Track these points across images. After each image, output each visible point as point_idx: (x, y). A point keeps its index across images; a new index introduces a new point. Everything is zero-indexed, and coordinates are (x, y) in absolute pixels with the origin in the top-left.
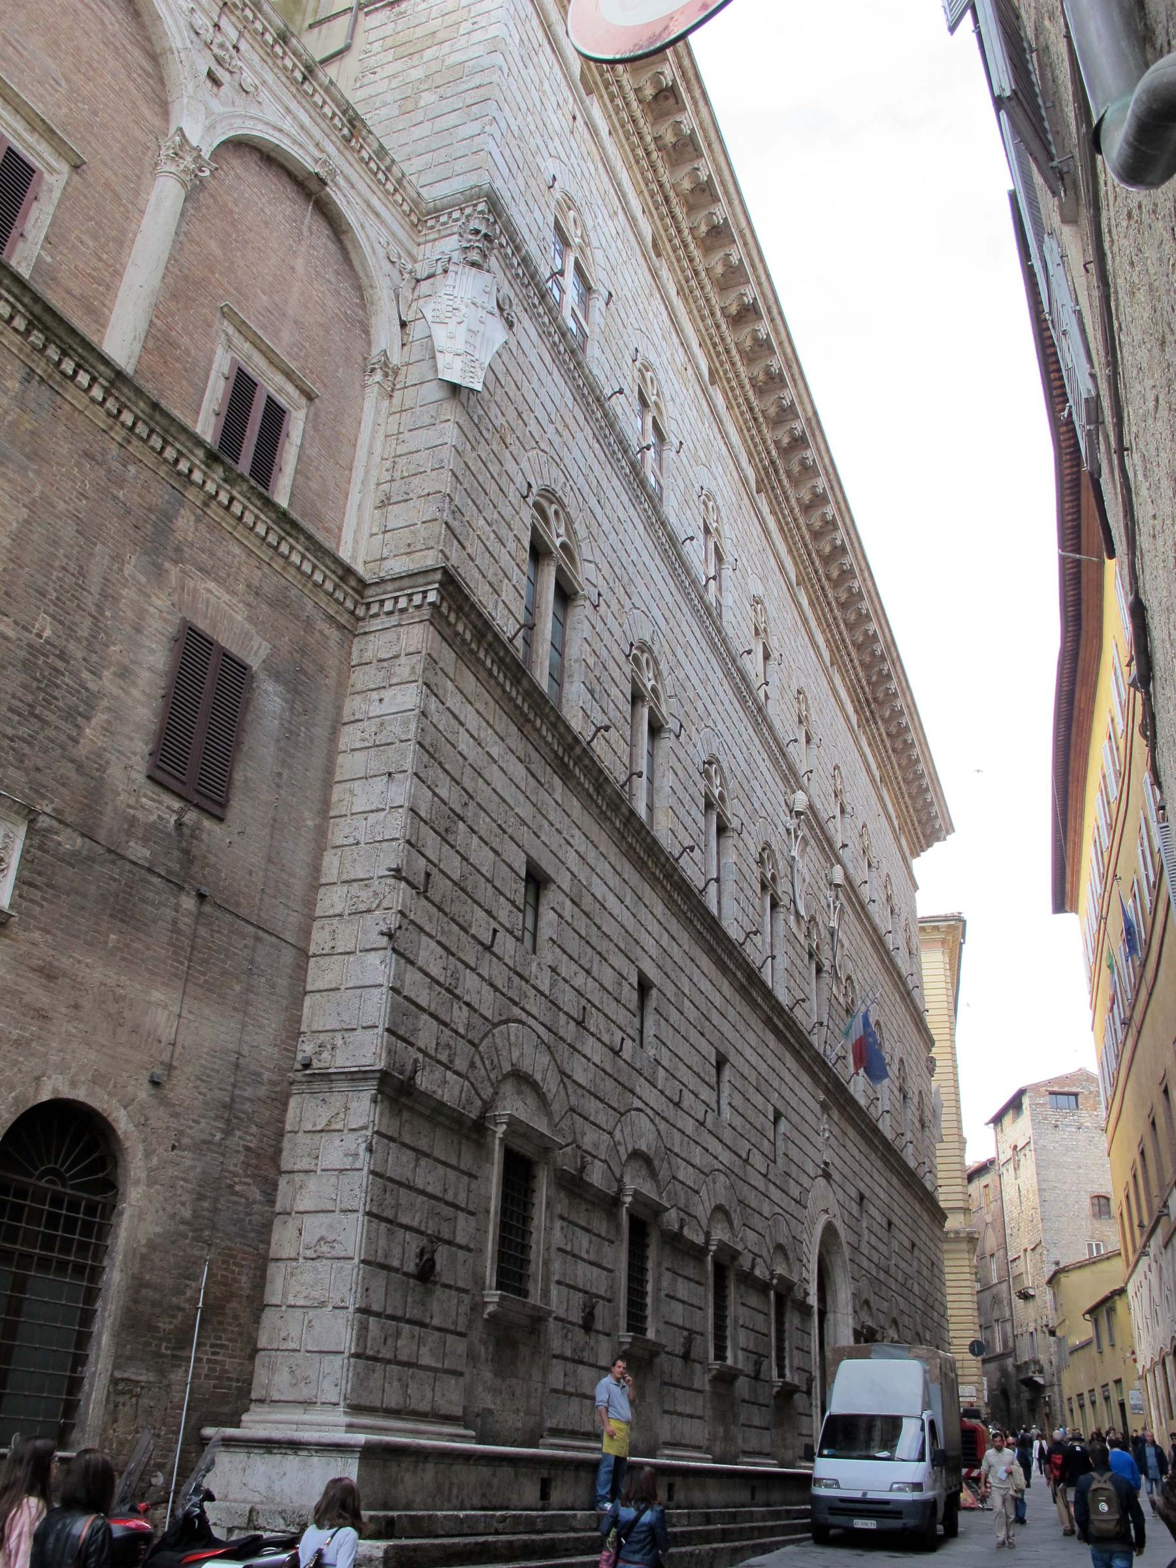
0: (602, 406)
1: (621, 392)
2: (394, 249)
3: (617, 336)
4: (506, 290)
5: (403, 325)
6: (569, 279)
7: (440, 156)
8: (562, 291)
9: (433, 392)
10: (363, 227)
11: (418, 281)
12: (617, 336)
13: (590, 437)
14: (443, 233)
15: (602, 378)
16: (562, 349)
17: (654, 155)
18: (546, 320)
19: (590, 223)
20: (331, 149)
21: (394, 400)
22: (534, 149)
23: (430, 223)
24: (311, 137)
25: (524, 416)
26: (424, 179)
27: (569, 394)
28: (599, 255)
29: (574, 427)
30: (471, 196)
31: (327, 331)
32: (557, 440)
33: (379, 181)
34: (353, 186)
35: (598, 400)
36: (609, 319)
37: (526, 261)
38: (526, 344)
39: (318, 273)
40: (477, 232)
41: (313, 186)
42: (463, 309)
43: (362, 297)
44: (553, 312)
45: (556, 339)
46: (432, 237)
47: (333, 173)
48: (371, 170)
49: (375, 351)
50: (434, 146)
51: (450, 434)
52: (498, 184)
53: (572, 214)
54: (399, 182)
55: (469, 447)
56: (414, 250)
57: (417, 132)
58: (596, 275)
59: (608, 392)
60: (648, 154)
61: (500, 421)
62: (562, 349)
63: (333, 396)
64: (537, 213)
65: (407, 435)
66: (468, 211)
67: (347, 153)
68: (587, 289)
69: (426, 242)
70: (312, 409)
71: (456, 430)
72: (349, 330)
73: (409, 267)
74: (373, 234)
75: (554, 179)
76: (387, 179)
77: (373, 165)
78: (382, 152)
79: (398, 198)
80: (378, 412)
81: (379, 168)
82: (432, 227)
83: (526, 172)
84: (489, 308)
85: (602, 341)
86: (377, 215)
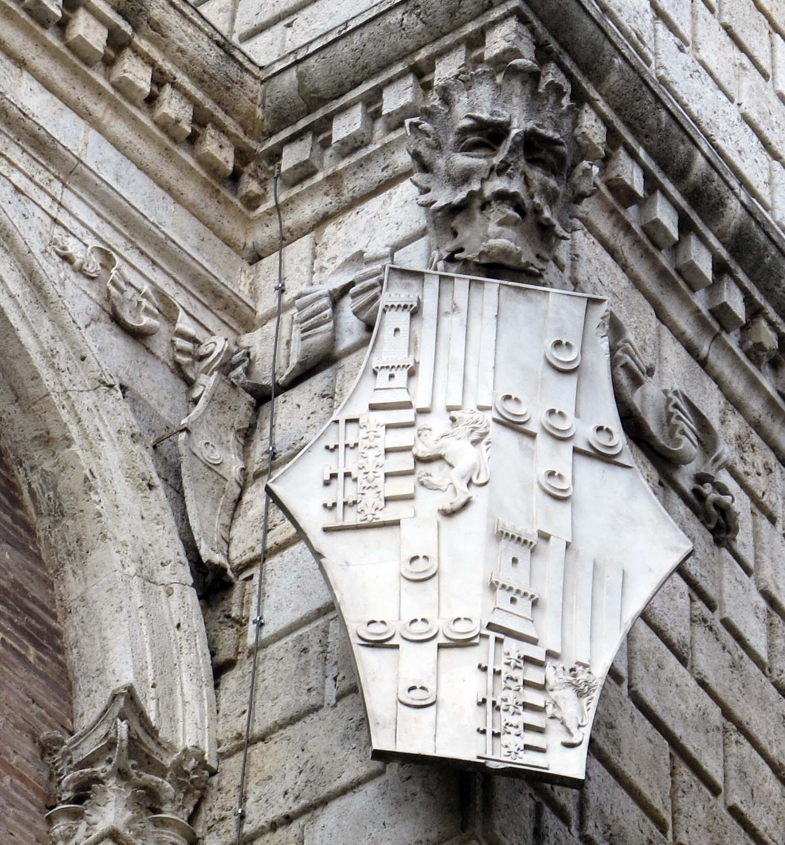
2: (139, 275)
4: (672, 373)
5: (213, 585)
11: (262, 397)
14: (354, 185)
23: (291, 158)
40: (488, 135)
42: (464, 454)
46: (306, 211)
49: (90, 706)
56: (239, 283)
66: (445, 70)
69: (286, 239)
73: (217, 344)
82: (305, 172)
84: (585, 435)
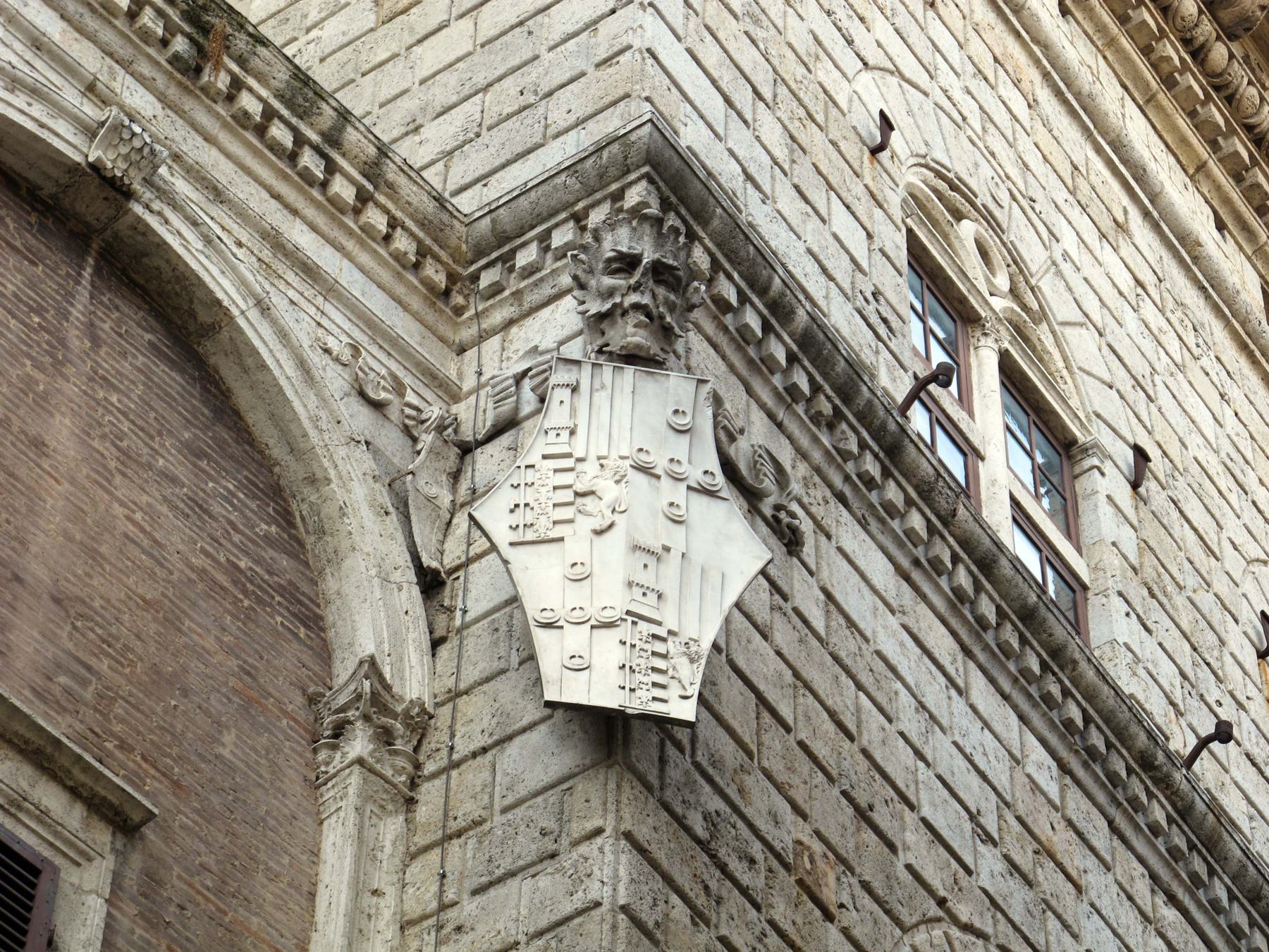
0: (1164, 783)
1: (1224, 733)
2: (378, 362)
3: (1191, 581)
4: (757, 432)
5: (431, 583)
6: (988, 417)
7: (505, 97)
8: (970, 452)
9: (537, 759)
10: (264, 308)
11: (466, 450)
12: (1191, 581)
13: (1142, 888)
14: (532, 298)
15: (1156, 707)
16: (987, 609)
17: (1219, 53)
18: (916, 521)
19: (1034, 255)
20: (139, 99)
21: (423, 812)
22: (804, 44)
23: (486, 280)
24: (68, 68)
25: (881, 817)
26: (461, 171)
27: (1037, 753)
28: (1083, 345)
29: (1078, 860)
30: (598, 175)
31: (172, 622)
32: (1017, 899)
33: (306, 176)
34: (217, 194)
35: (1146, 763)
36: (1151, 532)
37: (815, 345)
38: (857, 602)
39: (126, 455)
40: (627, 263)
41: (91, 206)
42: (609, 490)
43: (286, 518)
44: (945, 503)
45: (963, 578)
46: (497, 317)
47: (146, 158)
48: (275, 147)
49: (343, 670)
50: (480, 79)
51: (608, 872)
52: (692, 136)
53: (968, 230)
54: (373, 170)
55: (680, 911)
56: (450, 368)
57: (431, 56)
58: (1087, 401)
59: (1182, 743)
60: (1198, 53)
61: (790, 832)
62: (987, 609)
63: (207, 815)
64: (841, 221)
65: (470, 907)
67: (188, 104)
68: (1059, 449)
69: (483, 337)
70: (136, 860)
71: (626, 862)
72: (249, 617)
73: (434, 412)
74: (302, 333)
75: (886, 124)
76: (331, 168)
77: (278, 132)
78: (302, 91)
79: (377, 220)
80: (365, 852)
81: (300, 140)
82: (496, 289)
83: (787, 106)
85: (1137, 594)
86: (309, 271)
